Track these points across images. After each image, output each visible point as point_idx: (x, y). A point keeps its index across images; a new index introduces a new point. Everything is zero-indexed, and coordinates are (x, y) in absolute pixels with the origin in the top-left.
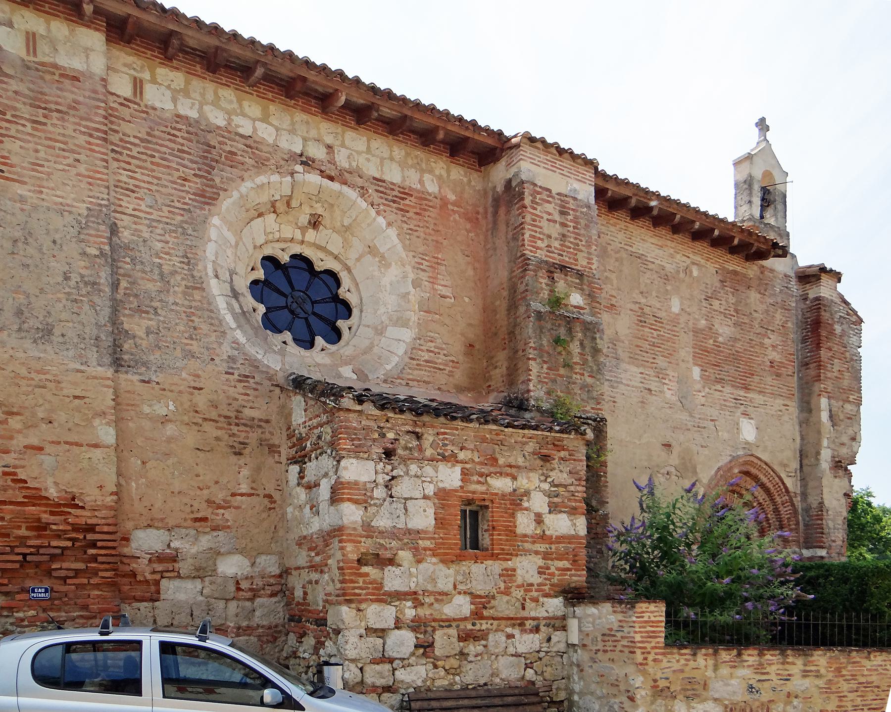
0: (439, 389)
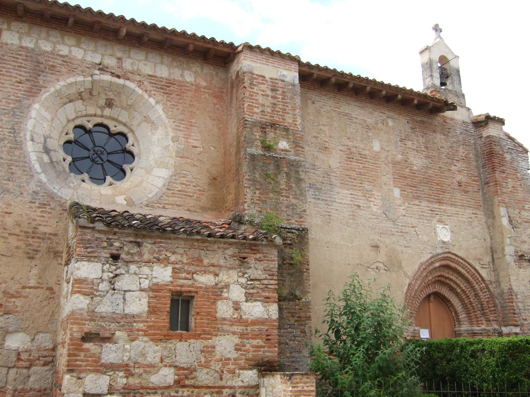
0: (188, 210)
